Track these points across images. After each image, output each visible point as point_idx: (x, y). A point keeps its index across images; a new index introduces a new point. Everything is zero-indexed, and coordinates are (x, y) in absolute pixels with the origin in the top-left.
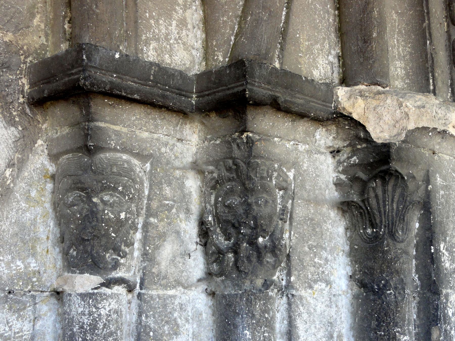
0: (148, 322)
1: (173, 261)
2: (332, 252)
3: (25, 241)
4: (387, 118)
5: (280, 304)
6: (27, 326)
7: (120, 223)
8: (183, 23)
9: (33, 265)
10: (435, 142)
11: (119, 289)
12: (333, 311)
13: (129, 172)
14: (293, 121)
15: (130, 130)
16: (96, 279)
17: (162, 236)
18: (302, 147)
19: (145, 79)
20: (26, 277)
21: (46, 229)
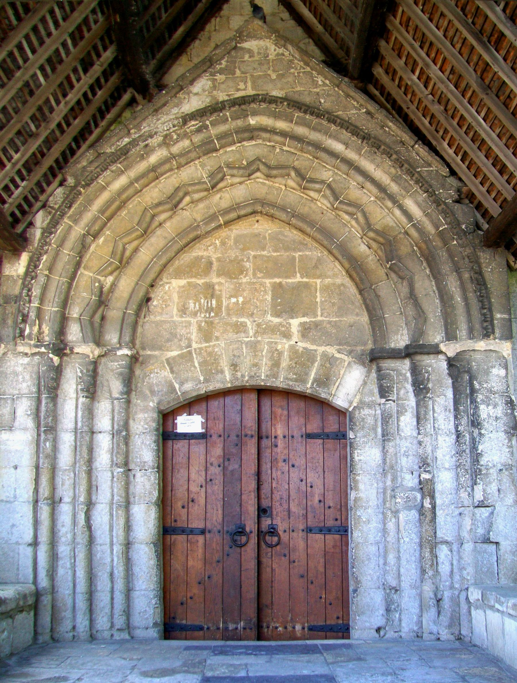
0: (8, 328)
1: (404, 394)
2: (446, 387)
3: (372, 394)
4: (451, 350)
5: (430, 402)
6: (374, 412)
7: (388, 387)
8: (402, 335)
9: (374, 399)
10: (472, 353)
11: (390, 402)
12: (447, 403)
13: (389, 374)
14: (157, 430)
15: (388, 364)
16: (384, 400)
17: (401, 389)
18: (433, 361)
19: (388, 353)
20: (372, 401)
21: (376, 391)
